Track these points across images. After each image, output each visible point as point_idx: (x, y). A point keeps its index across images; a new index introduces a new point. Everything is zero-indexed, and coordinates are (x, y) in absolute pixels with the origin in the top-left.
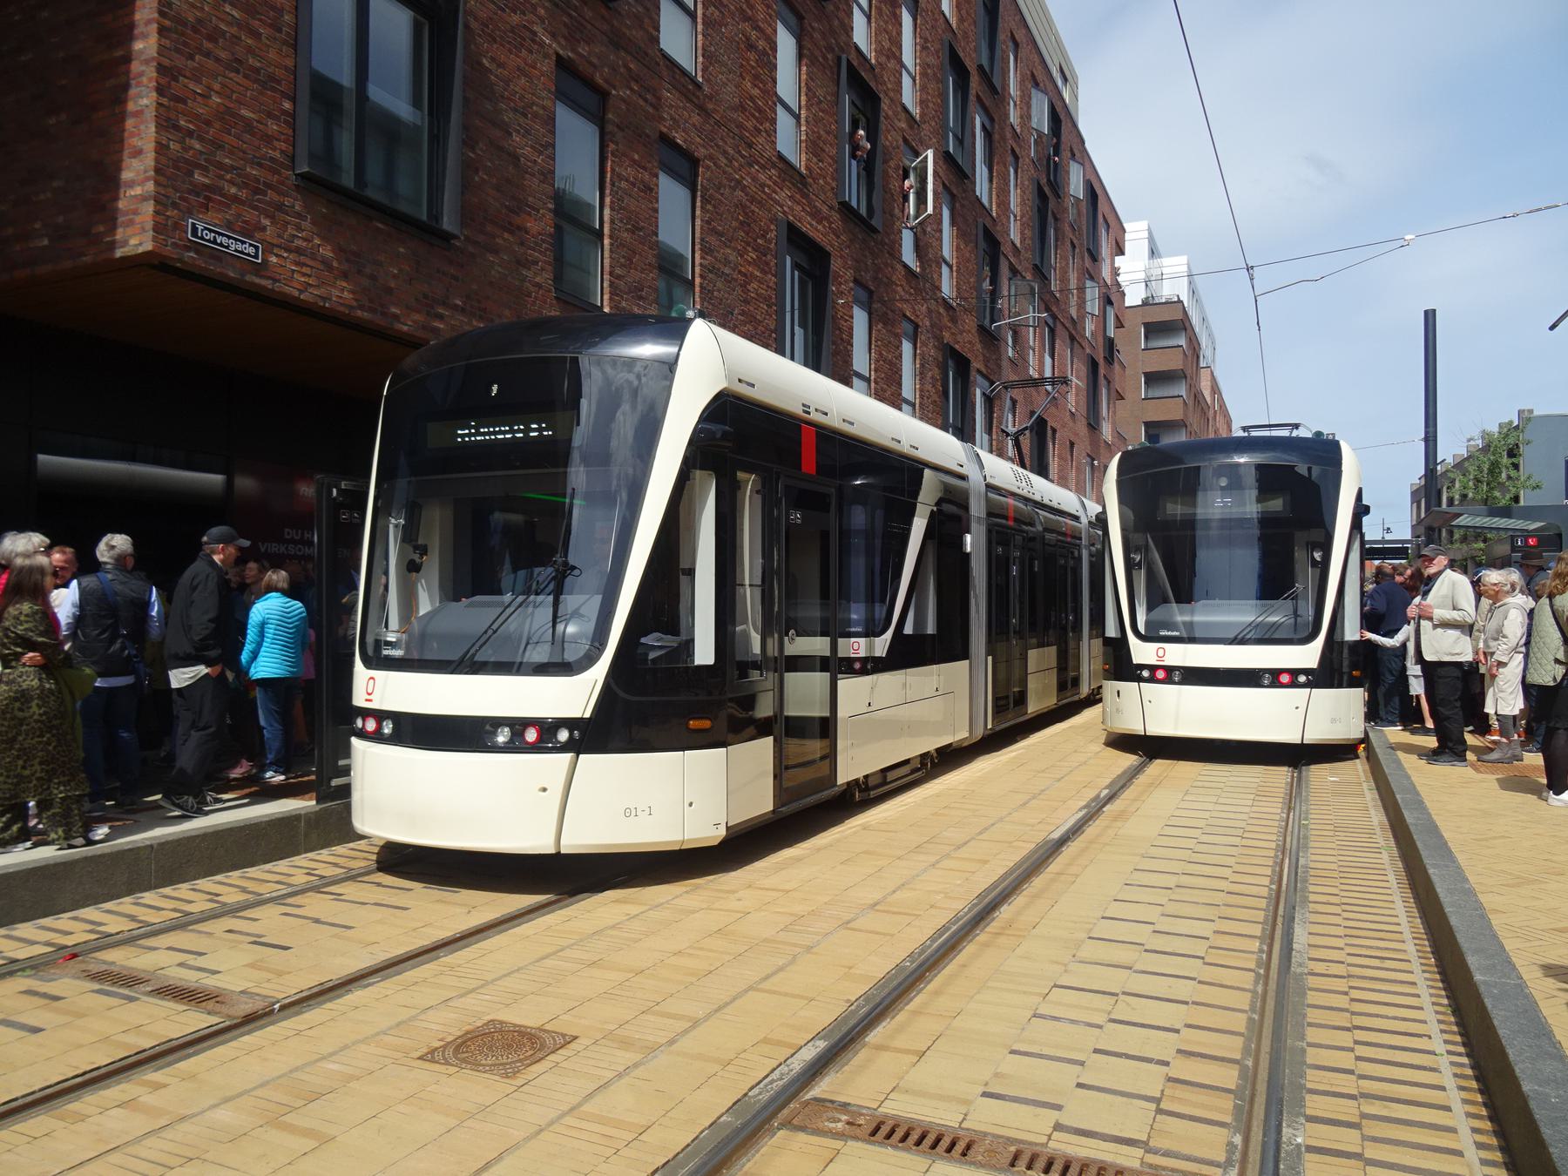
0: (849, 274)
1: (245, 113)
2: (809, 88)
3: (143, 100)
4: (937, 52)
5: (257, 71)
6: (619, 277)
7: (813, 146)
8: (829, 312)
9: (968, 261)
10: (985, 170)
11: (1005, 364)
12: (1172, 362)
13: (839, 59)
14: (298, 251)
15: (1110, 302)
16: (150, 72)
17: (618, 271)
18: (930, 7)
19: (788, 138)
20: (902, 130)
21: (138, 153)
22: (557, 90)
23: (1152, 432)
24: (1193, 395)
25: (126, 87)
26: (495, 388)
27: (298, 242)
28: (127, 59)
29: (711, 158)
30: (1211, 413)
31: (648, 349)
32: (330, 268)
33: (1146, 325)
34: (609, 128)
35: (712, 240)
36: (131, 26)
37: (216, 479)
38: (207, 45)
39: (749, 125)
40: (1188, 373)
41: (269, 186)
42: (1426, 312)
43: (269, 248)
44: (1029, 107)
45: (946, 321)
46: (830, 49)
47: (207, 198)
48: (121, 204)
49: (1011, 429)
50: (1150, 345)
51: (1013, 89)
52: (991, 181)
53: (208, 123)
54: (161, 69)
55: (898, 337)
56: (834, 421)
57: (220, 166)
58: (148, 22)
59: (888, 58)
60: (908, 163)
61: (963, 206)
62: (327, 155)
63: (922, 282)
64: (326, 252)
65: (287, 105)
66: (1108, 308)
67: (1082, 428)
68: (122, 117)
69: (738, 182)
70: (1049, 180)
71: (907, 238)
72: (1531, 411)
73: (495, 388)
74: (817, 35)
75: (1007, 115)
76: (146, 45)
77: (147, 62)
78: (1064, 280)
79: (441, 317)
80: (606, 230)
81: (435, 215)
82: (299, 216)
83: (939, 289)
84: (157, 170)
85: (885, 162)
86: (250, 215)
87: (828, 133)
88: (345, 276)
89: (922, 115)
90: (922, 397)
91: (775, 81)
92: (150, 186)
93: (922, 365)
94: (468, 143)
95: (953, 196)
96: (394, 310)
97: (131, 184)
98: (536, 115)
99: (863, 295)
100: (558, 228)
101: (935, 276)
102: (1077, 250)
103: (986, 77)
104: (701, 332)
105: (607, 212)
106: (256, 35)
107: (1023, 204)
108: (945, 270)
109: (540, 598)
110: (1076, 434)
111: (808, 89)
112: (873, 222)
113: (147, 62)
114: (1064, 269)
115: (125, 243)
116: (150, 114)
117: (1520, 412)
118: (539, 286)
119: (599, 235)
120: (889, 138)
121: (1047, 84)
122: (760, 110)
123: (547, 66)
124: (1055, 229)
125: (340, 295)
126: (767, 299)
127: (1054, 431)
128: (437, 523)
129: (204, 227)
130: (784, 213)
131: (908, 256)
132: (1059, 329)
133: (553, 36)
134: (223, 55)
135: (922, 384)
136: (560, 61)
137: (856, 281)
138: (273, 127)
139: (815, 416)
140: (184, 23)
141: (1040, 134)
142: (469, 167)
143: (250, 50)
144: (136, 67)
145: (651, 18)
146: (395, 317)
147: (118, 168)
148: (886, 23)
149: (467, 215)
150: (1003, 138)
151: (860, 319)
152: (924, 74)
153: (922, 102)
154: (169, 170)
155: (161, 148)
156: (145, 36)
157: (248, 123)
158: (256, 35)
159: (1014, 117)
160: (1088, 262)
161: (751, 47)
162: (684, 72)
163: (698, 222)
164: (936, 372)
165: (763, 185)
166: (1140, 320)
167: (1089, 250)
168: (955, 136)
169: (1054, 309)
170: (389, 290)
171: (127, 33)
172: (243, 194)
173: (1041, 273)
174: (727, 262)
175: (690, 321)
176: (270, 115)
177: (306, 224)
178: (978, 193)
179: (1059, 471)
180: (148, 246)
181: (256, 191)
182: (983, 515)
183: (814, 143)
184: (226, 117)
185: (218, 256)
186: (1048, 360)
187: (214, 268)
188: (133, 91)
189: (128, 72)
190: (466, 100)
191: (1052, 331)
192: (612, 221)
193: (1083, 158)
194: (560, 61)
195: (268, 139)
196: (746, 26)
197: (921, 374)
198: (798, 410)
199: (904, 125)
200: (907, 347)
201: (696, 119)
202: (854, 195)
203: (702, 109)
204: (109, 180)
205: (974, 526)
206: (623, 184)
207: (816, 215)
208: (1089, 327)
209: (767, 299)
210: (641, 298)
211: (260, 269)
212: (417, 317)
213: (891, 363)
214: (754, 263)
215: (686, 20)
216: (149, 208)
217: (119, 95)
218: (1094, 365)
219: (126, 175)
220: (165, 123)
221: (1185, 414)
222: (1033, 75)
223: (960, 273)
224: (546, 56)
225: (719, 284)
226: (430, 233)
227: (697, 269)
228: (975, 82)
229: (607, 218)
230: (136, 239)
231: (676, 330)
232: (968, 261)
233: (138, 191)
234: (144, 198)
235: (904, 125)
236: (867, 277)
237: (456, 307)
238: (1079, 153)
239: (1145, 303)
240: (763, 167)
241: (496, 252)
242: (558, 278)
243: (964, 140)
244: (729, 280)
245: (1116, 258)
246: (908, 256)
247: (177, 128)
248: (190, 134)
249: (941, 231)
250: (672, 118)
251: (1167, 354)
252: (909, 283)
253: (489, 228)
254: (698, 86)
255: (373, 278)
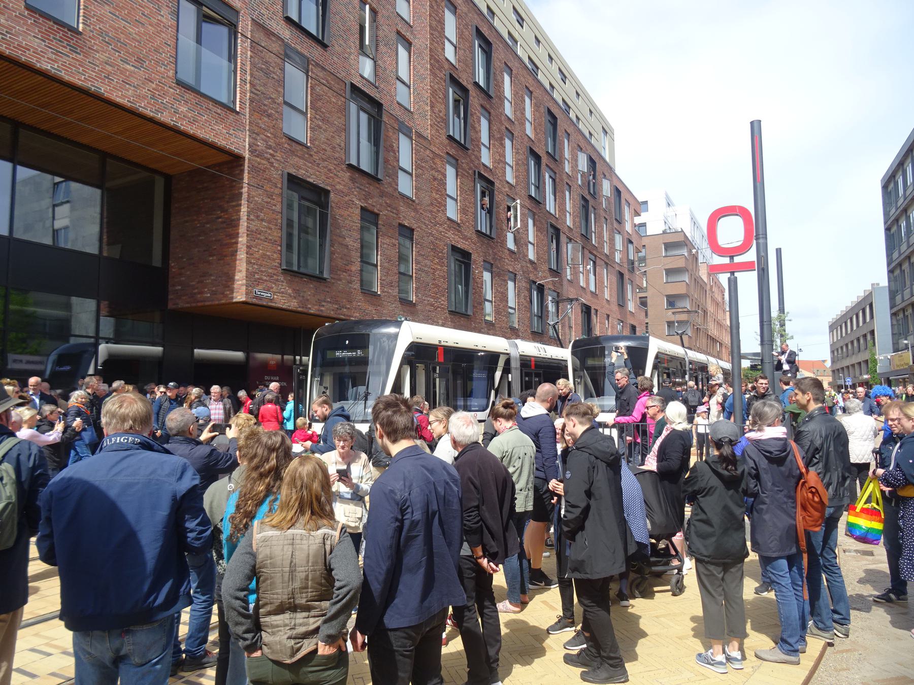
0: (481, 259)
1: (268, 253)
2: (461, 188)
3: (242, 255)
4: (524, 152)
5: (271, 240)
6: (384, 280)
7: (463, 211)
8: (471, 276)
9: (543, 240)
10: (552, 197)
11: (565, 283)
12: (681, 263)
13: (475, 172)
14: (283, 293)
15: (631, 242)
16: (244, 248)
17: (383, 278)
18: (519, 135)
19: (452, 211)
20: (506, 192)
21: (240, 271)
22: (361, 218)
23: (671, 300)
24: (693, 279)
25: (236, 251)
26: (347, 342)
27: (282, 290)
28: (237, 243)
29: (419, 227)
30: (708, 288)
31: (392, 330)
32: (291, 296)
33: (665, 244)
34: (379, 226)
35: (420, 258)
36: (238, 233)
37: (239, 355)
38: (259, 236)
39: (435, 210)
40: (690, 268)
41: (274, 274)
42: (777, 249)
43: (275, 293)
44: (576, 161)
45: (531, 269)
46: (470, 168)
47: (258, 282)
48: (235, 286)
49: (552, 323)
50: (668, 254)
51: (567, 154)
52: (555, 200)
53: (259, 259)
54: (248, 247)
55: (506, 282)
56: (450, 344)
57: (262, 271)
58: (244, 233)
59: (499, 163)
60: (509, 204)
61: (539, 216)
62: (289, 263)
63: (518, 255)
64: (290, 291)
65: (279, 248)
66: (630, 246)
67: (615, 307)
68: (235, 260)
69: (431, 233)
70: (589, 192)
71: (510, 237)
72: (878, 284)
73: (347, 342)
74: (464, 165)
75: (563, 169)
76: (243, 240)
77: (243, 245)
78: (600, 237)
79: (323, 306)
80: (379, 264)
81: (321, 272)
82: (282, 282)
83: (527, 256)
84: (246, 277)
85: (498, 208)
86: (269, 284)
87: (470, 203)
88: (295, 298)
89: (517, 182)
90: (518, 305)
91: (446, 190)
92: (244, 282)
93: (519, 291)
94: (332, 245)
95: (534, 214)
96: (309, 306)
97: (238, 280)
98: (354, 230)
99: (488, 266)
100: (362, 266)
101: (525, 251)
102: (608, 221)
103: (552, 157)
104: (406, 324)
105: (379, 257)
106: (271, 229)
107: (574, 206)
108: (530, 247)
109: (360, 402)
110: (611, 311)
111: (461, 189)
112: (492, 236)
113: (243, 245)
114: (600, 233)
115: (236, 298)
116: (244, 260)
117: (873, 285)
118: (355, 289)
119: (376, 266)
120: (498, 197)
121: (587, 147)
122: (439, 203)
123: (358, 211)
124: (595, 214)
125: (293, 304)
126: (443, 277)
127: (596, 311)
128: (328, 380)
129: (258, 290)
130: (451, 241)
131: (511, 244)
132: (598, 261)
133: (360, 200)
134: (262, 238)
135: (518, 299)
136: (362, 208)
137: (484, 261)
138: (275, 256)
139: (443, 344)
140: (252, 231)
141: (584, 173)
142: (332, 253)
143: (269, 234)
144: (239, 246)
145: (395, 182)
146: (310, 308)
147: (234, 275)
148: (497, 149)
149: (332, 271)
150: (562, 180)
151: (487, 276)
152: (517, 164)
153: (516, 177)
154: (250, 275)
155: (247, 270)
156: (242, 237)
157: (269, 256)
158: (271, 229)
159: (567, 168)
160: (616, 225)
161: (435, 179)
162: (408, 198)
163: (414, 253)
164: (527, 293)
165: (441, 232)
166: (661, 241)
167: (616, 219)
168: (535, 186)
169: (595, 252)
170: (308, 300)
171: (237, 235)
172: (267, 279)
173: (586, 237)
174: (426, 266)
175: (402, 321)
176: (275, 252)
177: (284, 284)
178: (548, 209)
179: (600, 330)
180: (244, 299)
181: (272, 277)
182: (518, 365)
183: (463, 209)
184: (264, 256)
185: (261, 299)
186: (592, 277)
187: (260, 302)
188: (238, 253)
189: (237, 247)
190: (331, 231)
191: (594, 263)
192: (381, 260)
193: (611, 176)
194: (362, 208)
195: (274, 260)
196: (433, 172)
197: (518, 295)
198: (437, 343)
199: (507, 189)
200: (511, 285)
201: (413, 214)
202: (484, 228)
203: (416, 210)
204: (230, 278)
205: (513, 371)
206: (385, 246)
207: (465, 238)
208: (618, 257)
209: (443, 277)
210: (392, 286)
211: (271, 300)
212: (316, 307)
213: (502, 293)
214: (438, 263)
215: (409, 177)
216: (244, 288)
217: (234, 254)
218: (621, 275)
219: (237, 277)
220: (249, 262)
221: (688, 290)
222: (579, 146)
223: (537, 246)
224: (357, 208)
225: (423, 275)
226: (320, 279)
227: (414, 271)
228: (545, 160)
229: (379, 259)
230: (240, 296)
231: (398, 324)
232: (543, 240)
233: (240, 282)
234: (242, 285)
235: (507, 189)
236: (490, 259)
237: (328, 302)
238: (610, 171)
239: (664, 232)
240: (441, 225)
241: (340, 280)
242: (362, 285)
243: (540, 187)
244: (427, 272)
245: (635, 218)
246: (511, 244)
247: (251, 263)
248: (254, 264)
249: (528, 230)
250: (404, 217)
251: (678, 259)
252: (511, 257)
253: (339, 272)
254: (414, 201)
255: (303, 297)
